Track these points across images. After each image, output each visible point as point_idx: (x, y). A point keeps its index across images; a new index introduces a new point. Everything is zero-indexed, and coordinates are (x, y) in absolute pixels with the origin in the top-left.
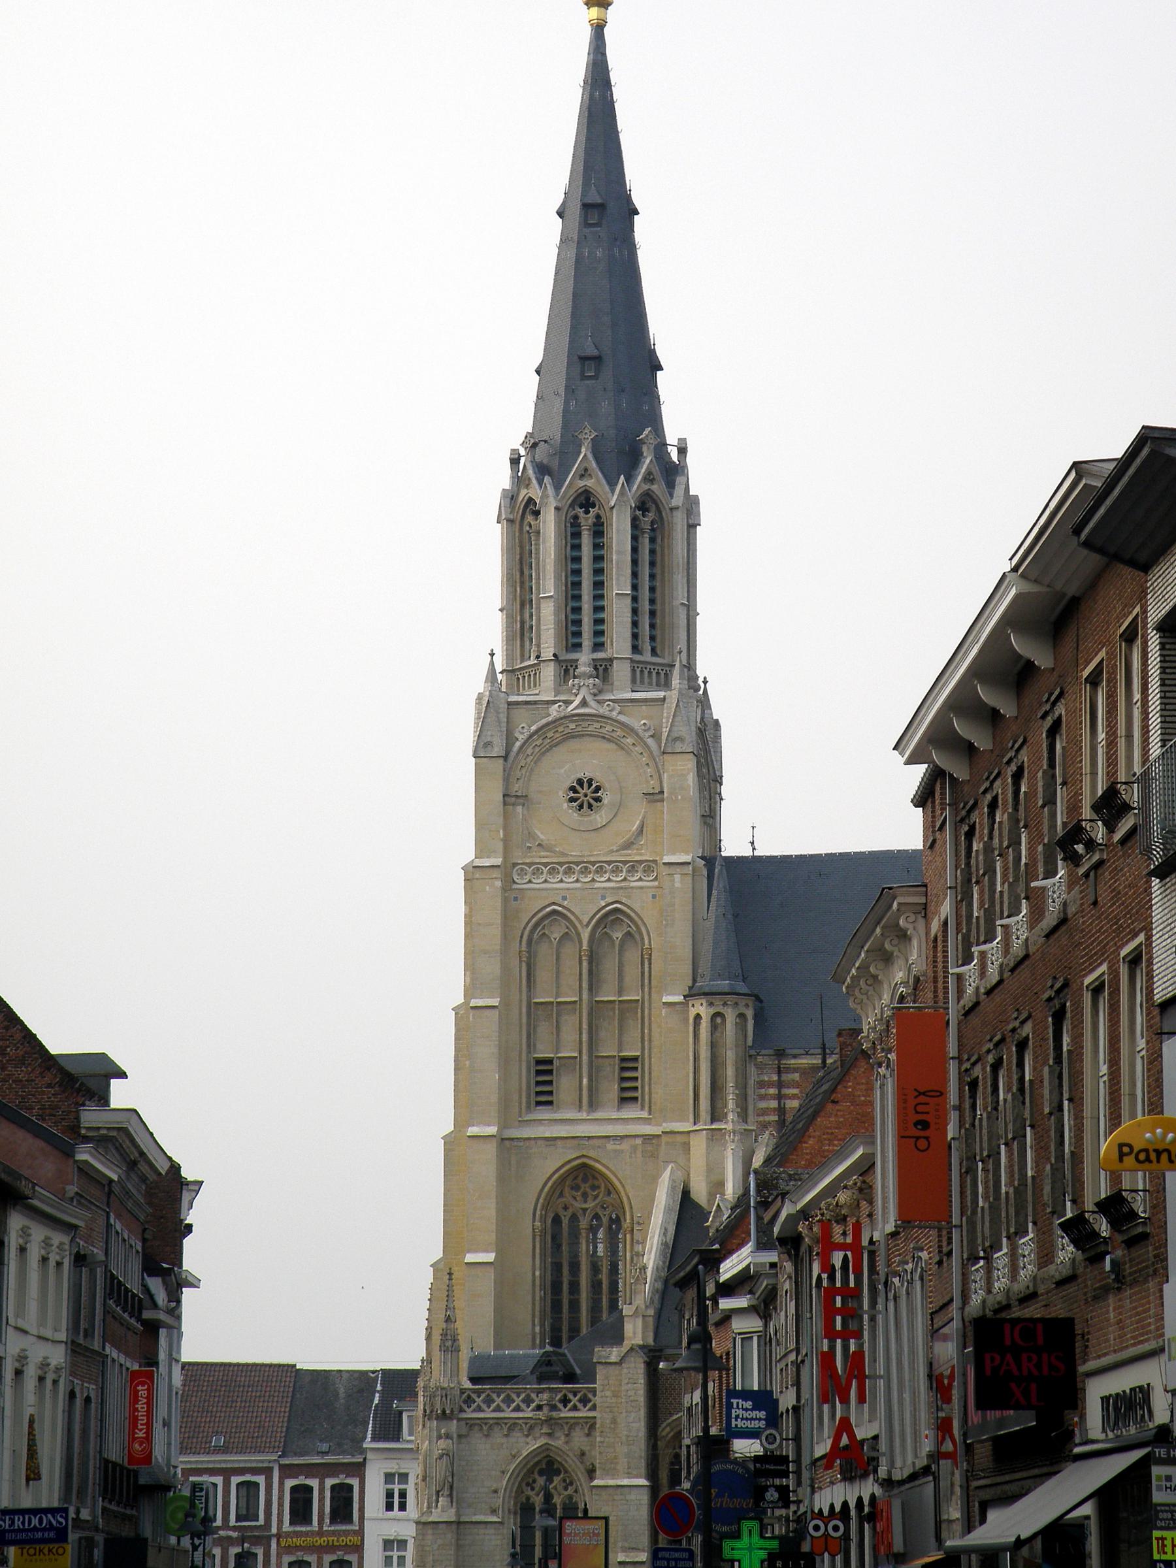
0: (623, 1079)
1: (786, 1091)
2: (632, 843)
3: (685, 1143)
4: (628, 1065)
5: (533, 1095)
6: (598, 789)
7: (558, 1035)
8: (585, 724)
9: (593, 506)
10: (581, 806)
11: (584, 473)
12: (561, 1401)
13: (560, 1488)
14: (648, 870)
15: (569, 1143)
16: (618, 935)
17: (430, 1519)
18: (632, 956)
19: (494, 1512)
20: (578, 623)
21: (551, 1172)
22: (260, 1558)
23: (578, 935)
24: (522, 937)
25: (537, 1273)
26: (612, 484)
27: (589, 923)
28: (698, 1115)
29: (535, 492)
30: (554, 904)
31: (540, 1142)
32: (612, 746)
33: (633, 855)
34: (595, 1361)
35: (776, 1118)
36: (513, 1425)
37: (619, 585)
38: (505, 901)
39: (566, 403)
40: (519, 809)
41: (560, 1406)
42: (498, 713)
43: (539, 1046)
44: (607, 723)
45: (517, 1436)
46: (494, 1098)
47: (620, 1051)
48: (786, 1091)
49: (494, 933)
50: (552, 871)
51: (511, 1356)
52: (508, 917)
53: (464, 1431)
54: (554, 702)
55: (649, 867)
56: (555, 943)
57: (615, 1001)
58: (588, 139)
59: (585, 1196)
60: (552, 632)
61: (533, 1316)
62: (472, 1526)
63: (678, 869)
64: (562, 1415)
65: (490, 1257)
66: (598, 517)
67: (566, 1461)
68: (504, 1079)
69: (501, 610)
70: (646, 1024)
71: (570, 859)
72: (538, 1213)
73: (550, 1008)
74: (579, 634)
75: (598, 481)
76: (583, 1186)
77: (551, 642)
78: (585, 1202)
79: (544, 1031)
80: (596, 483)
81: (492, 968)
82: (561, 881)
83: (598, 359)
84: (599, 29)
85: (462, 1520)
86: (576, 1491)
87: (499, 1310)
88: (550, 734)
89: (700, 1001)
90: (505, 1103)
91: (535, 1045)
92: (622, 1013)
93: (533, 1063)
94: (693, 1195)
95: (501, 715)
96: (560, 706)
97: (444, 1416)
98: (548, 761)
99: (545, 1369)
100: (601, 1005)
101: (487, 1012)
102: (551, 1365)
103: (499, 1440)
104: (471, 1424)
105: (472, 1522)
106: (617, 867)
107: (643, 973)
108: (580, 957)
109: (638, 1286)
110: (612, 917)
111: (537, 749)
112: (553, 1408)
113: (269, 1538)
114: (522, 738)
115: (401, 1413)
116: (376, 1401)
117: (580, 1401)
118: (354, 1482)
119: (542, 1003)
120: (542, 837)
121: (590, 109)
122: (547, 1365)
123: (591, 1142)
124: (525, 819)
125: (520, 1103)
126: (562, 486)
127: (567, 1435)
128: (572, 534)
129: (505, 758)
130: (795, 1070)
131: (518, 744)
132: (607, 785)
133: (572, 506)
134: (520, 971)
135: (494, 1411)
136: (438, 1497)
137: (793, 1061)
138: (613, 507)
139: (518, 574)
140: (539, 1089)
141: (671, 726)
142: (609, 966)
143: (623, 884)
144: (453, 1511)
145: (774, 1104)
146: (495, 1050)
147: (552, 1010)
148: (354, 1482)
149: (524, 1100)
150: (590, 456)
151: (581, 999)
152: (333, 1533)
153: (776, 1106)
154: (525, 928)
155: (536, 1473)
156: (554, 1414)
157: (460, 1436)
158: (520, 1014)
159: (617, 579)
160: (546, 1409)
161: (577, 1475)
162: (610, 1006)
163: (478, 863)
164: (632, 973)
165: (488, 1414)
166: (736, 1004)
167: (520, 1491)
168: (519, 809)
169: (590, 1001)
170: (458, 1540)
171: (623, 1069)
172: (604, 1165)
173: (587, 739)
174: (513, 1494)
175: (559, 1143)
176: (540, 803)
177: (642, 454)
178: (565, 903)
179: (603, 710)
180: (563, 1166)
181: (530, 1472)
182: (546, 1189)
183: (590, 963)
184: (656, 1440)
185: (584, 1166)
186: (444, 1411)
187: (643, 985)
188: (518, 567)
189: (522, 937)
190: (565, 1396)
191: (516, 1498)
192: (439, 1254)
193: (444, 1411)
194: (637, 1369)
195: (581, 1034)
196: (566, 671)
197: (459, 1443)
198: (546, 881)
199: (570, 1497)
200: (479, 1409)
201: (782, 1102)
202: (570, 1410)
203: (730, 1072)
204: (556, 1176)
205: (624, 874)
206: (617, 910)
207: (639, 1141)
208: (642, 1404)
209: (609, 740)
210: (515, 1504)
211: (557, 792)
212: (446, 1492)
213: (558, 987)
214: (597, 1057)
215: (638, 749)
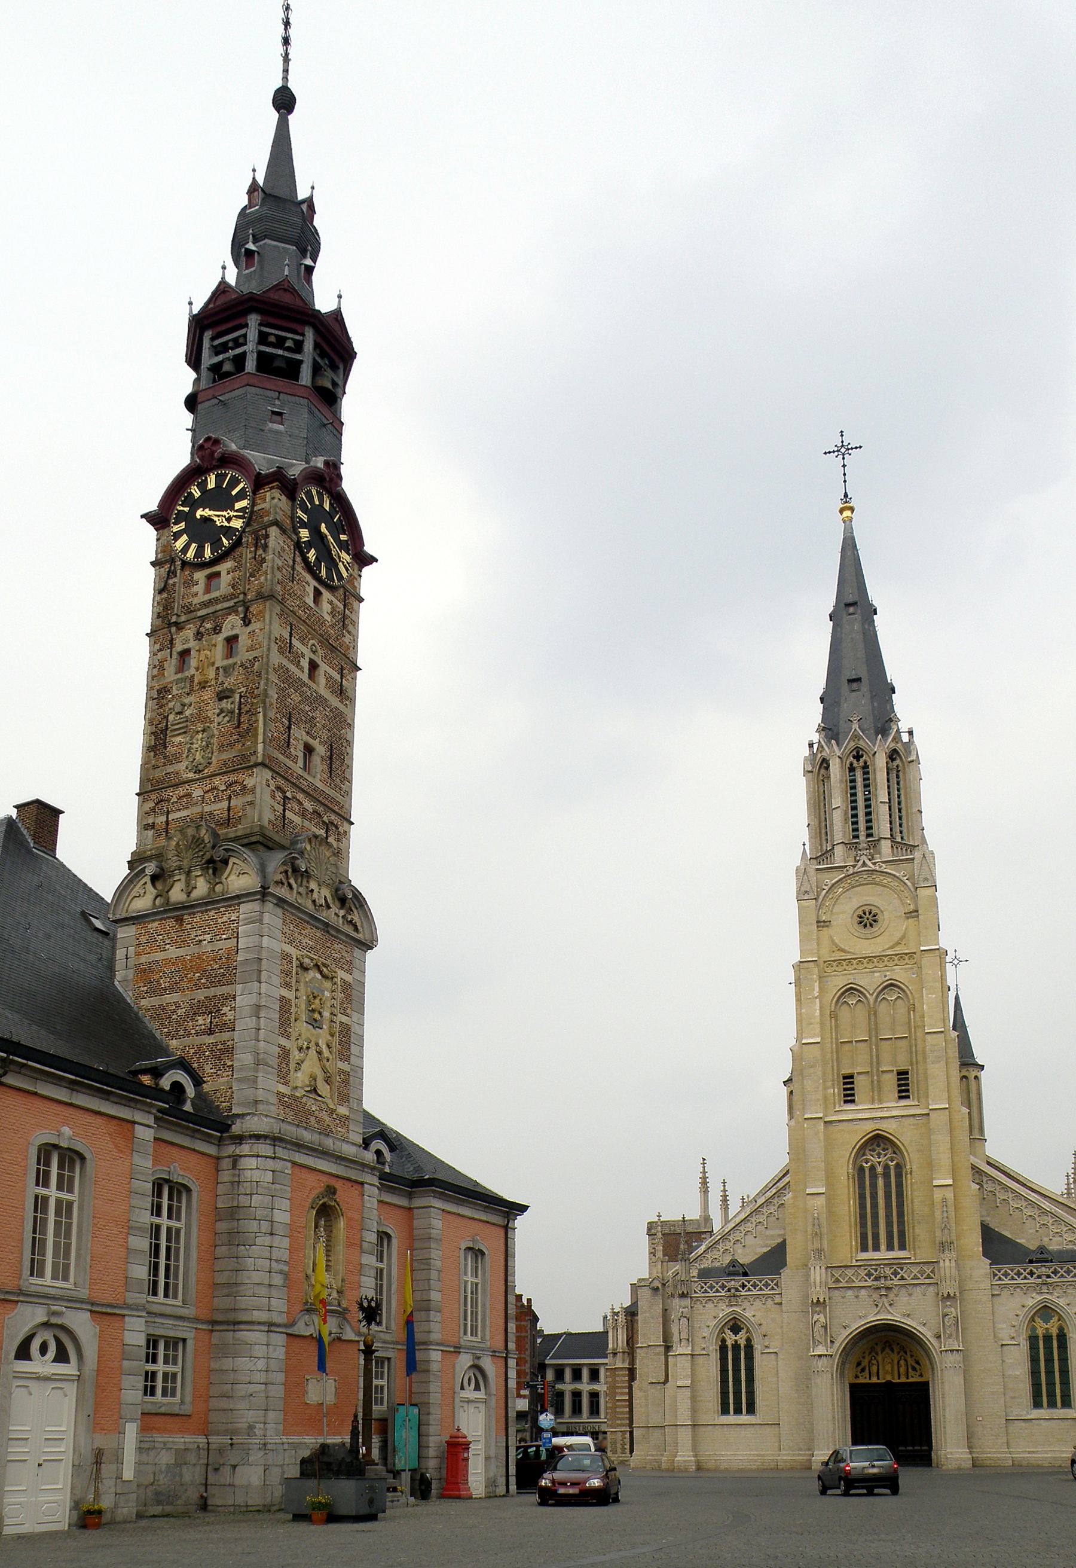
4: (902, 1075)
33: (900, 949)
41: (741, 1289)
44: (888, 877)
80: (865, 743)
83: (859, 680)
112: (1048, 1276)
118: (518, 1445)
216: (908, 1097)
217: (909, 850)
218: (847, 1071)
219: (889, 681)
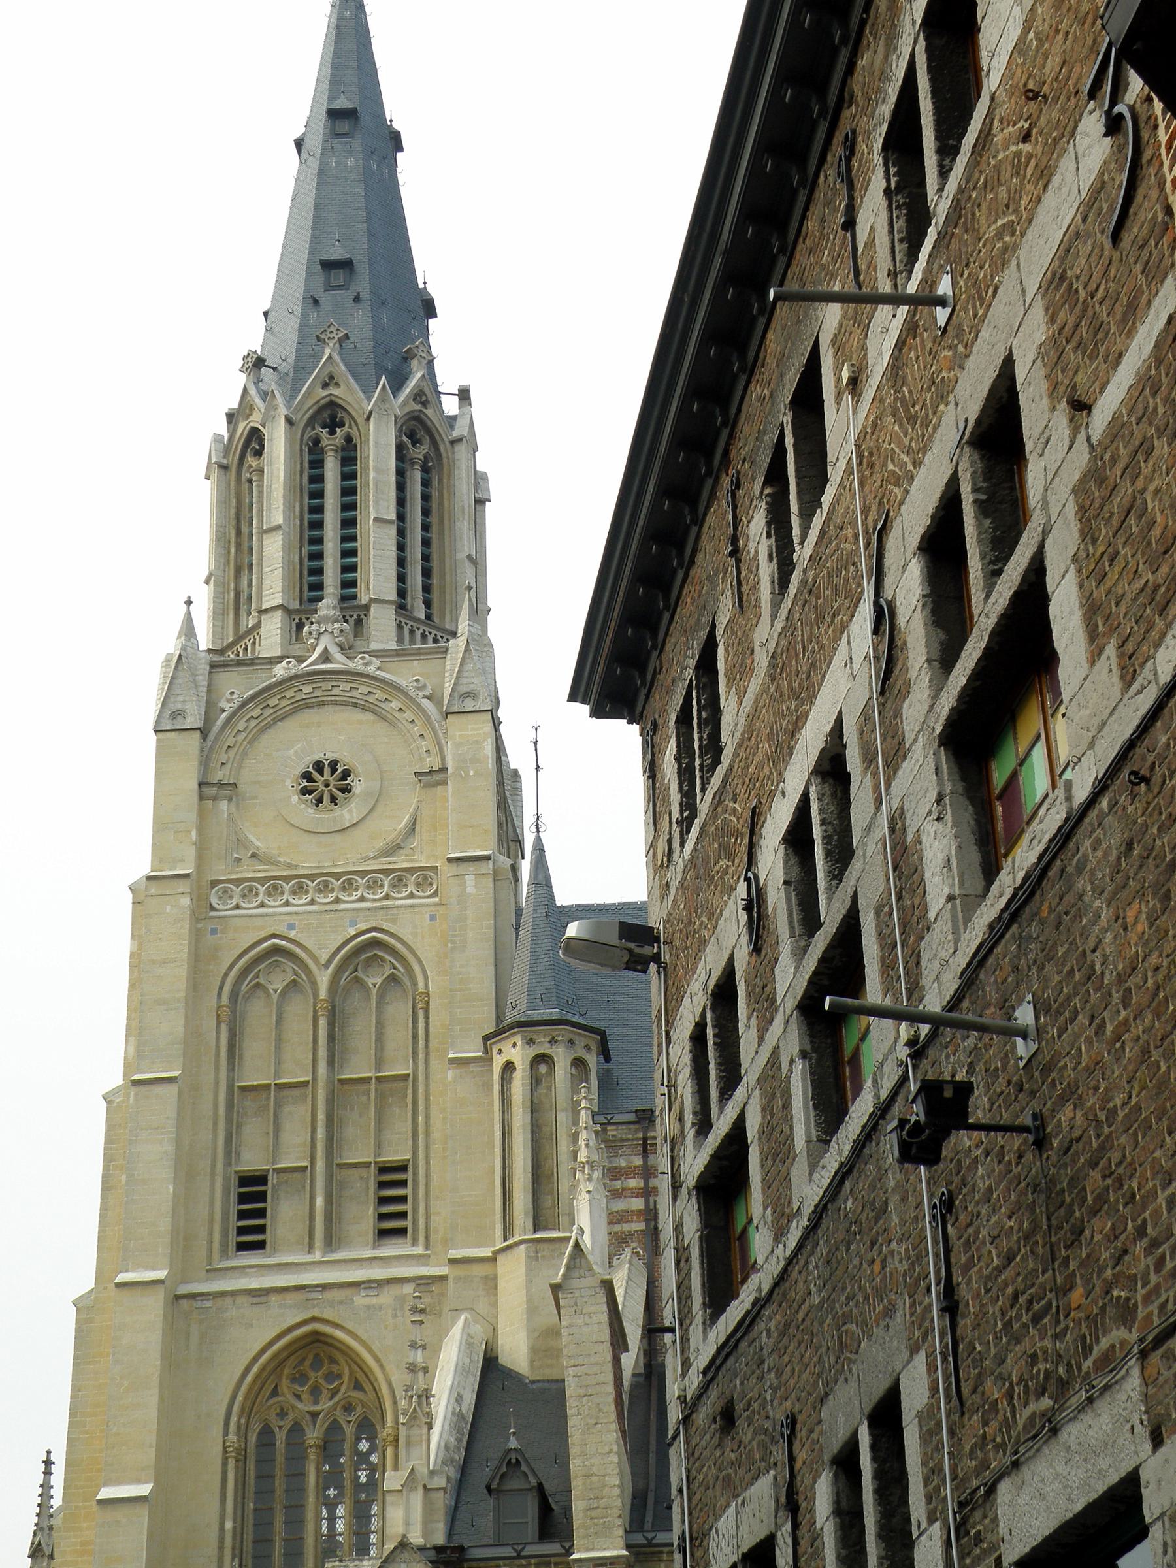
0: (382, 1201)
2: (399, 847)
3: (486, 1277)
5: (233, 1232)
6: (346, 774)
9: (342, 425)
10: (320, 800)
11: (329, 381)
16: (374, 980)
18: (399, 1010)
23: (314, 983)
24: (221, 987)
25: (229, 1525)
26: (368, 392)
27: (329, 961)
28: (511, 1224)
30: (274, 936)
31: (240, 1300)
32: (370, 716)
35: (642, 1226)
39: (304, 315)
43: (246, 1155)
44: (360, 683)
46: (165, 1225)
49: (176, 977)
50: (274, 891)
52: (199, 959)
54: (279, 660)
56: (275, 997)
57: (371, 1078)
59: (315, 1392)
60: (279, 573)
63: (471, 867)
65: (144, 1490)
66: (349, 439)
70: (421, 1108)
71: (301, 872)
72: (234, 1419)
73: (264, 1095)
74: (319, 586)
76: (312, 1374)
77: (278, 586)
79: (254, 1132)
80: (348, 393)
82: (287, 904)
83: (346, 265)
88: (273, 702)
91: (238, 1154)
92: (381, 1096)
93: (234, 1182)
94: (504, 1360)
96: (289, 662)
98: (267, 739)
101: (159, 1089)
107: (415, 1036)
108: (315, 1012)
109: (415, 1431)
114: (229, 707)
120: (258, 843)
121: (338, 28)
123: (329, 1295)
124: (231, 819)
128: (311, 462)
129: (204, 732)
132: (360, 769)
133: (310, 423)
134: (218, 1038)
138: (371, 413)
139: (233, 532)
140: (259, 1237)
141: (458, 677)
143: (383, 903)
145: (638, 1204)
146: (170, 1148)
147: (268, 1099)
149: (217, 1237)
150: (336, 357)
151: (315, 1079)
153: (642, 1207)
154: (226, 975)
158: (216, 1106)
159: (376, 502)
162: (362, 1088)
164: (398, 1035)
168: (223, 805)
169: (330, 1082)
171: (382, 1185)
173: (330, 708)
175: (273, 1298)
176: (256, 798)
179: (357, 664)
180: (279, 1337)
182: (249, 1378)
183: (331, 1024)
185: (316, 1338)
187: (415, 1053)
188: (233, 523)
189: (221, 987)
196: (300, 626)
198: (262, 905)
201: (652, 1199)
207: (408, 1289)
209: (364, 709)
211: (284, 781)
215: (409, 715)
216: (402, 1232)
217: (418, 634)
218: (252, 1162)
219: (421, 286)
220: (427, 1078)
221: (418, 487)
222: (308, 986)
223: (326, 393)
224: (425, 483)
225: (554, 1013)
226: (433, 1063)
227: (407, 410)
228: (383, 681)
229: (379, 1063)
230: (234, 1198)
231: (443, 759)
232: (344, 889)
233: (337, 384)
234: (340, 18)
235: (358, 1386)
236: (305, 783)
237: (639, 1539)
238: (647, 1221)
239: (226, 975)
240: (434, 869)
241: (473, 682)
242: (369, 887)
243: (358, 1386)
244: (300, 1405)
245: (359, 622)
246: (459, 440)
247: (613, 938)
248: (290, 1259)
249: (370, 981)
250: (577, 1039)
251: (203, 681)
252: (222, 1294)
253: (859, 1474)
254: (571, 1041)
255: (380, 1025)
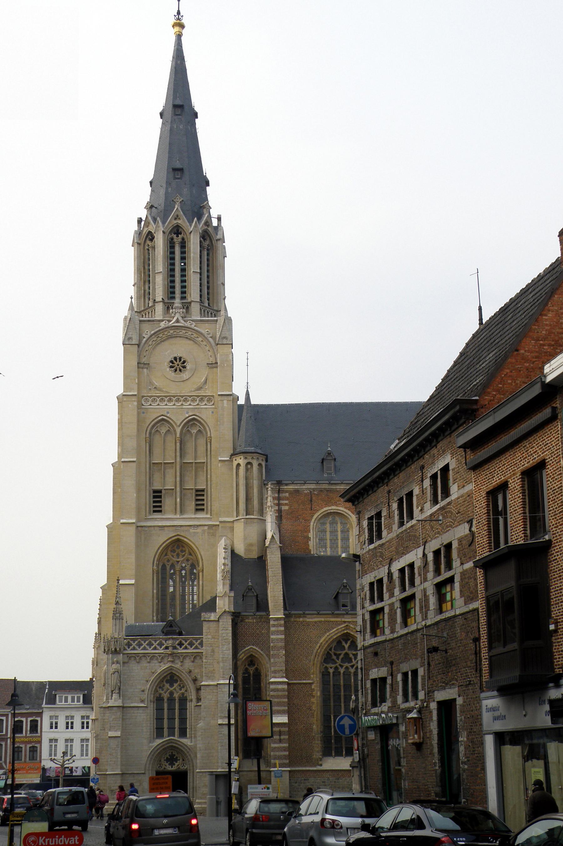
0: (197, 500)
1: (282, 502)
2: (201, 388)
4: (200, 493)
5: (152, 507)
6: (184, 362)
7: (164, 479)
8: (178, 331)
9: (181, 234)
10: (176, 370)
11: (177, 217)
12: (178, 645)
13: (177, 689)
14: (209, 400)
15: (171, 528)
16: (194, 431)
17: (109, 705)
18: (201, 441)
19: (142, 701)
20: (173, 287)
21: (162, 542)
22: (4, 746)
23: (175, 431)
24: (146, 431)
25: (155, 591)
29: (152, 228)
30: (162, 415)
31: (156, 528)
32: (191, 342)
33: (202, 393)
34: (202, 619)
36: (153, 657)
37: (194, 266)
38: (138, 414)
39: (167, 188)
40: (145, 370)
41: (178, 647)
42: (135, 325)
43: (155, 484)
45: (155, 663)
46: (134, 506)
47: (195, 486)
48: (282, 502)
49: (133, 428)
50: (162, 400)
51: (148, 626)
53: (126, 660)
54: (162, 321)
55: (210, 399)
56: (163, 435)
58: (175, 80)
60: (161, 289)
61: (153, 612)
62: (130, 709)
63: (225, 398)
64: (179, 651)
65: (133, 582)
66: (183, 239)
67: (181, 675)
68: (138, 498)
69: (134, 285)
72: (155, 562)
74: (173, 293)
75: (184, 221)
76: (177, 550)
78: (178, 558)
79: (157, 477)
80: (183, 222)
81: (132, 443)
82: (166, 405)
83: (181, 170)
84: (179, 37)
85: (125, 705)
86: (186, 691)
87: (136, 608)
88: (161, 335)
89: (240, 457)
90: (138, 510)
93: (152, 492)
94: (237, 551)
95: (136, 326)
97: (116, 652)
98: (159, 348)
99: (169, 629)
100: (185, 465)
102: (172, 627)
103: (145, 665)
104: (130, 656)
105: (131, 707)
106: (194, 399)
107: (207, 450)
108: (176, 440)
110: (192, 422)
111: (154, 342)
112: (175, 648)
113: (7, 738)
114: (147, 337)
115: (56, 695)
116: (46, 691)
117: (189, 644)
118: (39, 719)
119: (157, 463)
121: (175, 68)
122: (170, 627)
123: (182, 528)
124: (148, 375)
125: (146, 510)
126: (166, 222)
127: (182, 662)
129: (138, 345)
130: (287, 492)
131: (145, 339)
132: (189, 360)
133: (170, 233)
135: (142, 649)
136: (112, 694)
137: (285, 487)
138: (191, 232)
140: (154, 504)
142: (190, 446)
143: (197, 407)
144: (121, 701)
148: (39, 719)
150: (179, 209)
151: (176, 462)
152: (31, 737)
154: (148, 427)
155: (164, 681)
156: (175, 651)
157: (124, 663)
159: (194, 265)
160: (170, 648)
161: (187, 682)
162: (190, 465)
163: (125, 393)
164: (201, 449)
165: (139, 651)
166: (258, 458)
167: (156, 691)
170: (123, 716)
171: (197, 495)
172: (188, 539)
173: (178, 338)
174: (153, 692)
175: (166, 528)
177: (203, 213)
178: (168, 415)
179: (188, 324)
181: (162, 681)
182: (159, 551)
184: (237, 661)
185: (178, 540)
186: (116, 649)
187: (207, 455)
189: (146, 431)
190: (181, 642)
191: (154, 694)
192: (105, 582)
193: (116, 649)
194: (227, 622)
195: (176, 478)
196: (168, 308)
197: (124, 666)
198: (158, 405)
199: (183, 694)
200: (134, 649)
202: (183, 649)
203: (256, 491)
204: (164, 545)
205: (197, 402)
206: (194, 419)
207: (206, 528)
208: (231, 641)
209: (190, 339)
210: (154, 697)
212: (117, 691)
213: (164, 456)
214: (184, 489)
215: (205, 343)
216: (203, 510)
218: (157, 487)
220: (211, 464)
221: (206, 257)
222: (173, 432)
223: (175, 222)
224: (208, 255)
225: (252, 449)
226: (213, 459)
227: (203, 229)
228: (197, 331)
229: (196, 458)
230: (152, 497)
231: (216, 359)
232: (184, 401)
233: (179, 219)
234: (176, 64)
235: (190, 554)
236: (171, 364)
237: (287, 612)
238: (279, 514)
239: (148, 427)
240: (213, 396)
241: (227, 334)
242: (192, 401)
243: (190, 554)
244: (174, 559)
245: (188, 308)
246: (219, 240)
247: (352, 557)
248: (170, 517)
249: (192, 431)
250: (259, 458)
251: (138, 327)
252: (151, 526)
253: (408, 678)
254: (258, 458)
255: (196, 446)
